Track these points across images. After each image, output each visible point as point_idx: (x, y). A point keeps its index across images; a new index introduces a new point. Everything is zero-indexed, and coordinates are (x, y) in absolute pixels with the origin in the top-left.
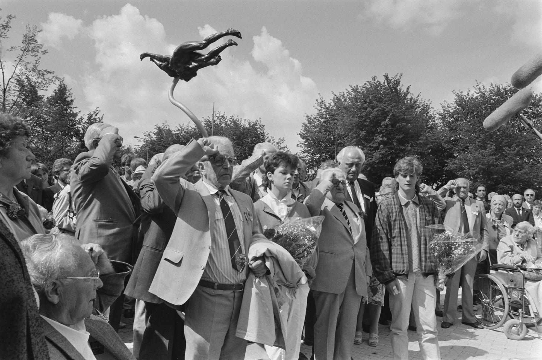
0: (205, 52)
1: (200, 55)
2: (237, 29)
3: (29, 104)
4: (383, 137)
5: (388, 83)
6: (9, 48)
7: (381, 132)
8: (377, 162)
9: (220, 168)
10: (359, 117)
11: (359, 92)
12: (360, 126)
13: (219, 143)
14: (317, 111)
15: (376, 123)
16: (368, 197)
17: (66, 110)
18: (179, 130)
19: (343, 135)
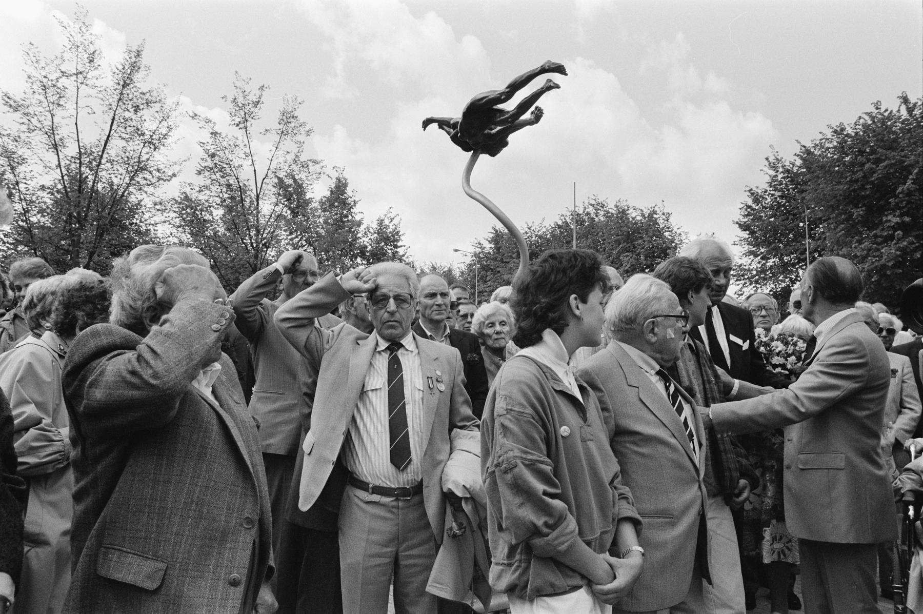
0: (510, 106)
1: (502, 112)
2: (557, 60)
3: (295, 213)
4: (901, 216)
5: (910, 111)
6: (263, 131)
7: (897, 206)
8: (890, 264)
9: (383, 311)
10: (851, 181)
11: (848, 135)
12: (853, 199)
13: (385, 272)
14: (768, 179)
15: (885, 189)
16: (739, 341)
17: (346, 216)
19: (820, 219)
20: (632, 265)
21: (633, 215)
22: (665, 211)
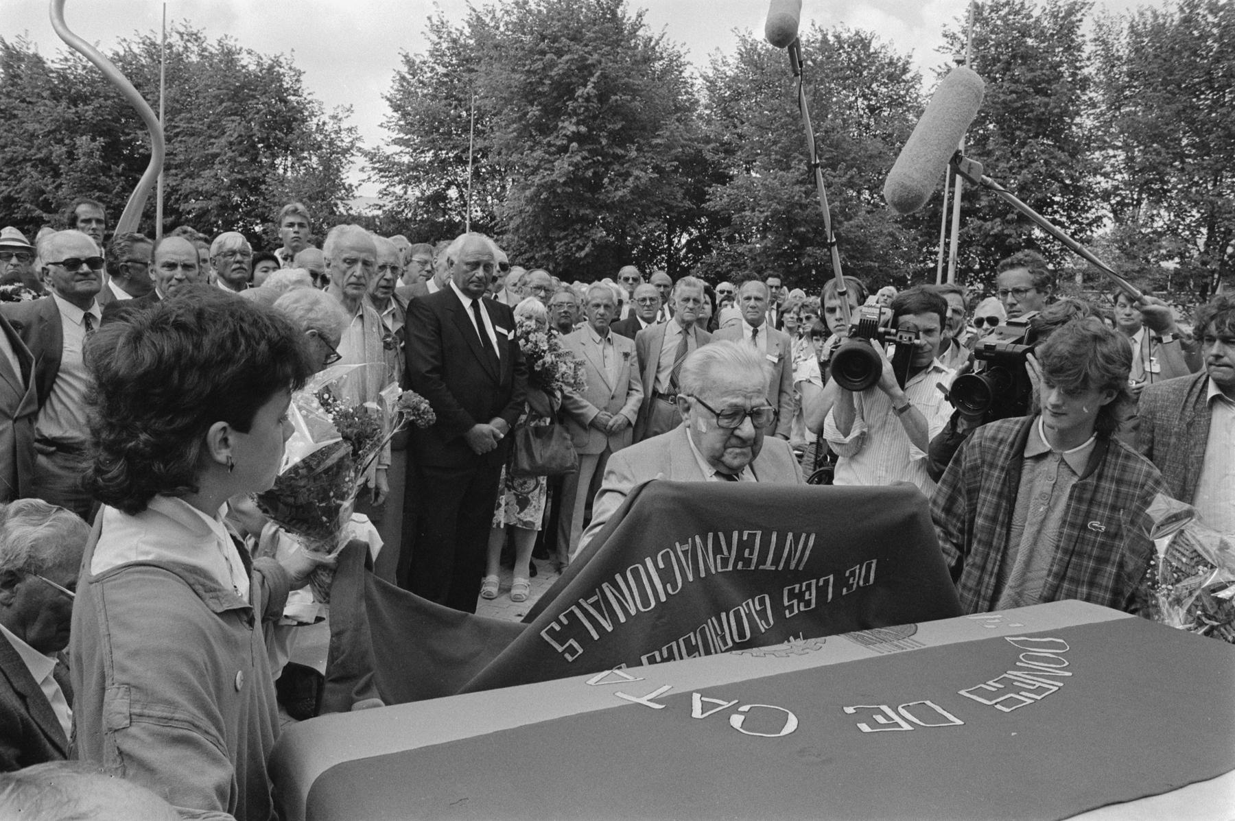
8: (562, 180)
14: (429, 46)
16: (505, 332)
18: (66, 60)
20: (240, 136)
21: (244, 63)
22: (293, 66)
